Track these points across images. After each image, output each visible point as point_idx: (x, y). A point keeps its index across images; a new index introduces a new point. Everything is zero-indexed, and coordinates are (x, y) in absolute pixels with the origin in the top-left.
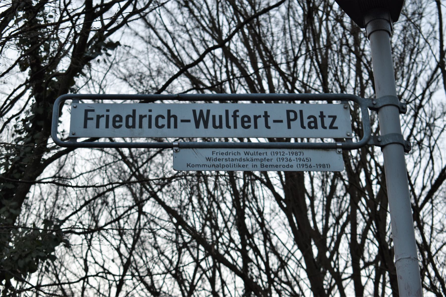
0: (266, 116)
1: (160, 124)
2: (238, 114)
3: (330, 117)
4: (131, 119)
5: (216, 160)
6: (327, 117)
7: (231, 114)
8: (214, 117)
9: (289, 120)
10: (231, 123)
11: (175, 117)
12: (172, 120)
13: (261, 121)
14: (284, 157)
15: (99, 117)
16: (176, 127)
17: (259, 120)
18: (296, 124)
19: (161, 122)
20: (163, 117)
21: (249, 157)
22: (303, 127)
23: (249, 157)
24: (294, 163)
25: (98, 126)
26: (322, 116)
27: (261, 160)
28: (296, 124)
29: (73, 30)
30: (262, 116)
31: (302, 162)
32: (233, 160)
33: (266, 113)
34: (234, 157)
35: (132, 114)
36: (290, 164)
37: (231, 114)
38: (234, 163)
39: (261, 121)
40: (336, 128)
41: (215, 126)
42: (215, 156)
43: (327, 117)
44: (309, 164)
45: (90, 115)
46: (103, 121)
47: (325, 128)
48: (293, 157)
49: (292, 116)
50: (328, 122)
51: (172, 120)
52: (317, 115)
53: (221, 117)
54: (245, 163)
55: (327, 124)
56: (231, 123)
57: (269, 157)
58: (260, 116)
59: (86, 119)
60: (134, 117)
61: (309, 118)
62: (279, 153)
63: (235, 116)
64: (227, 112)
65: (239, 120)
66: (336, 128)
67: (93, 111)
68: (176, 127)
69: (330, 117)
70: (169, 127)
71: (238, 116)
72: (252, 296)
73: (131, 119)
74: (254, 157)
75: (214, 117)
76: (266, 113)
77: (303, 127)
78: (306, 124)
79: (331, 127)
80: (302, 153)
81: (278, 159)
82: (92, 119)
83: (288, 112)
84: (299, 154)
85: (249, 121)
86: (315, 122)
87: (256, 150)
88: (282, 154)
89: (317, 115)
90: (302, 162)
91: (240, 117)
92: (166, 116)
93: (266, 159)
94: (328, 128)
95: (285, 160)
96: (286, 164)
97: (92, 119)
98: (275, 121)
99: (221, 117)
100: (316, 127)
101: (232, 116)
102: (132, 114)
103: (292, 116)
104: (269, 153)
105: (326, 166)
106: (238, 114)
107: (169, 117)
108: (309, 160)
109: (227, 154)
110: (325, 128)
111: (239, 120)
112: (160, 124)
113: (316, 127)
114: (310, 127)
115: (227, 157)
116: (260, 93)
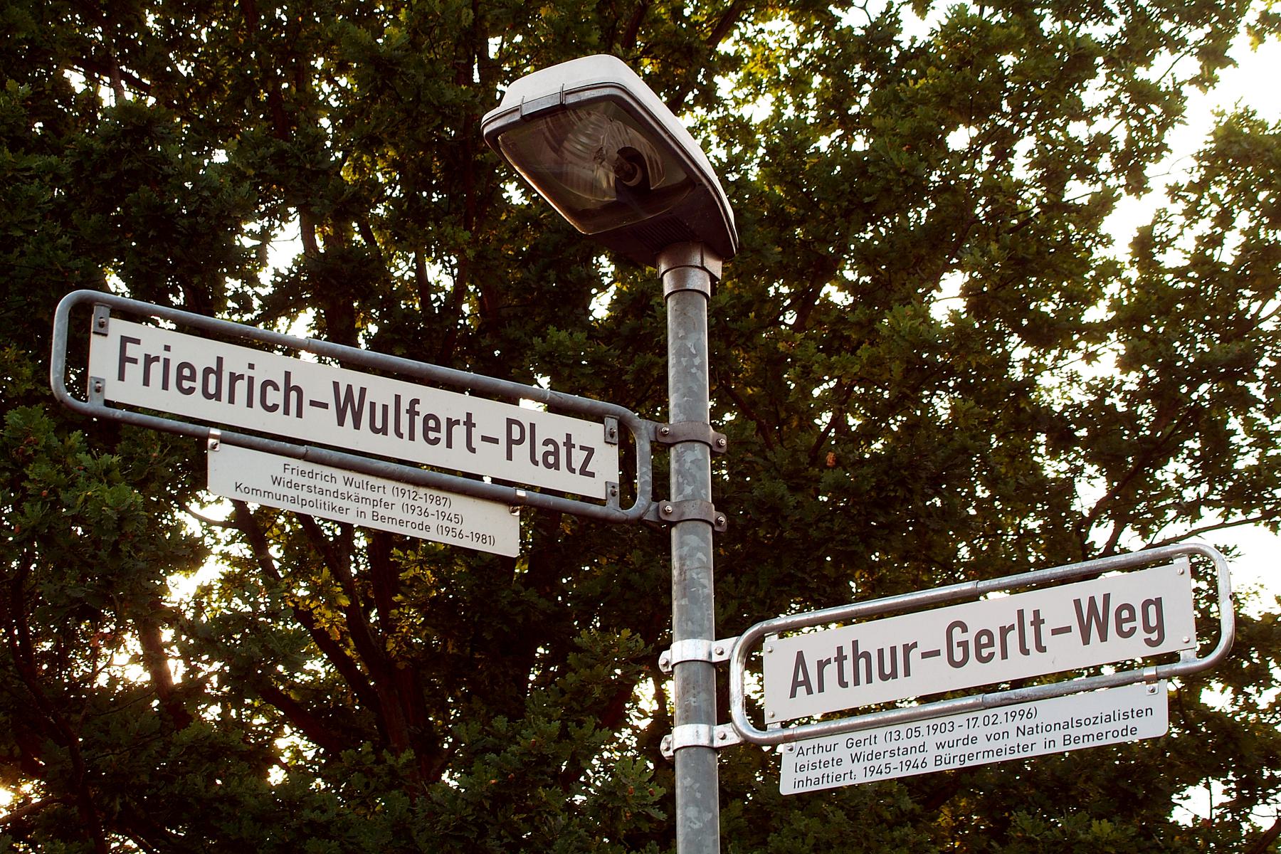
0: (469, 424)
1: (269, 404)
2: (417, 408)
3: (582, 448)
4: (212, 378)
5: (290, 484)
6: (577, 447)
7: (405, 405)
8: (373, 405)
9: (510, 442)
10: (405, 429)
11: (299, 391)
12: (293, 395)
13: (459, 432)
14: (416, 504)
15: (149, 360)
16: (299, 414)
17: (455, 428)
18: (521, 451)
19: (274, 397)
20: (276, 388)
21: (352, 490)
22: (536, 463)
23: (352, 490)
24: (432, 521)
25: (146, 382)
26: (569, 445)
27: (375, 503)
28: (521, 451)
29: (1151, 446)
30: (462, 423)
31: (446, 523)
32: (321, 492)
33: (469, 415)
34: (325, 486)
35: (215, 368)
36: (427, 521)
37: (405, 405)
38: (324, 498)
39: (459, 432)
40: (592, 475)
41: (374, 429)
42: (288, 476)
43: (577, 447)
44: (458, 528)
45: (132, 350)
46: (156, 369)
47: (573, 471)
48: (432, 508)
49: (516, 434)
50: (578, 457)
51: (293, 395)
52: (561, 440)
53: (385, 407)
54: (345, 504)
55: (577, 464)
56: (405, 429)
57: (388, 498)
58: (457, 422)
59: (124, 359)
60: (219, 373)
61: (546, 442)
62: (407, 493)
63: (412, 413)
64: (398, 398)
65: (419, 421)
66: (592, 475)
67: (137, 342)
68: (299, 414)
69: (582, 448)
70: (287, 412)
71: (418, 414)
72: (12, 780)
73: (212, 378)
74: (363, 493)
75: (373, 405)
76: (469, 415)
77: (536, 463)
78: (539, 457)
79: (584, 472)
80: (448, 502)
81: (405, 507)
82: (135, 361)
83: (510, 422)
84: (443, 501)
85: (192, 378)
86: (556, 453)
87: (366, 478)
88: (413, 495)
89: (561, 440)
90: (446, 523)
91: (422, 415)
92: (282, 386)
93: (384, 501)
94: (578, 472)
95: (417, 510)
96: (418, 520)
97: (135, 361)
98: (484, 439)
99: (385, 407)
100: (556, 466)
101: (408, 411)
102: (215, 368)
103: (516, 434)
104: (389, 490)
105: (488, 539)
106: (417, 408)
107: (288, 389)
108: (458, 519)
109: (312, 475)
110: (573, 471)
111: (419, 421)
112: (269, 404)
113: (556, 466)
114: (548, 466)
115: (312, 482)
116: (363, 346)
